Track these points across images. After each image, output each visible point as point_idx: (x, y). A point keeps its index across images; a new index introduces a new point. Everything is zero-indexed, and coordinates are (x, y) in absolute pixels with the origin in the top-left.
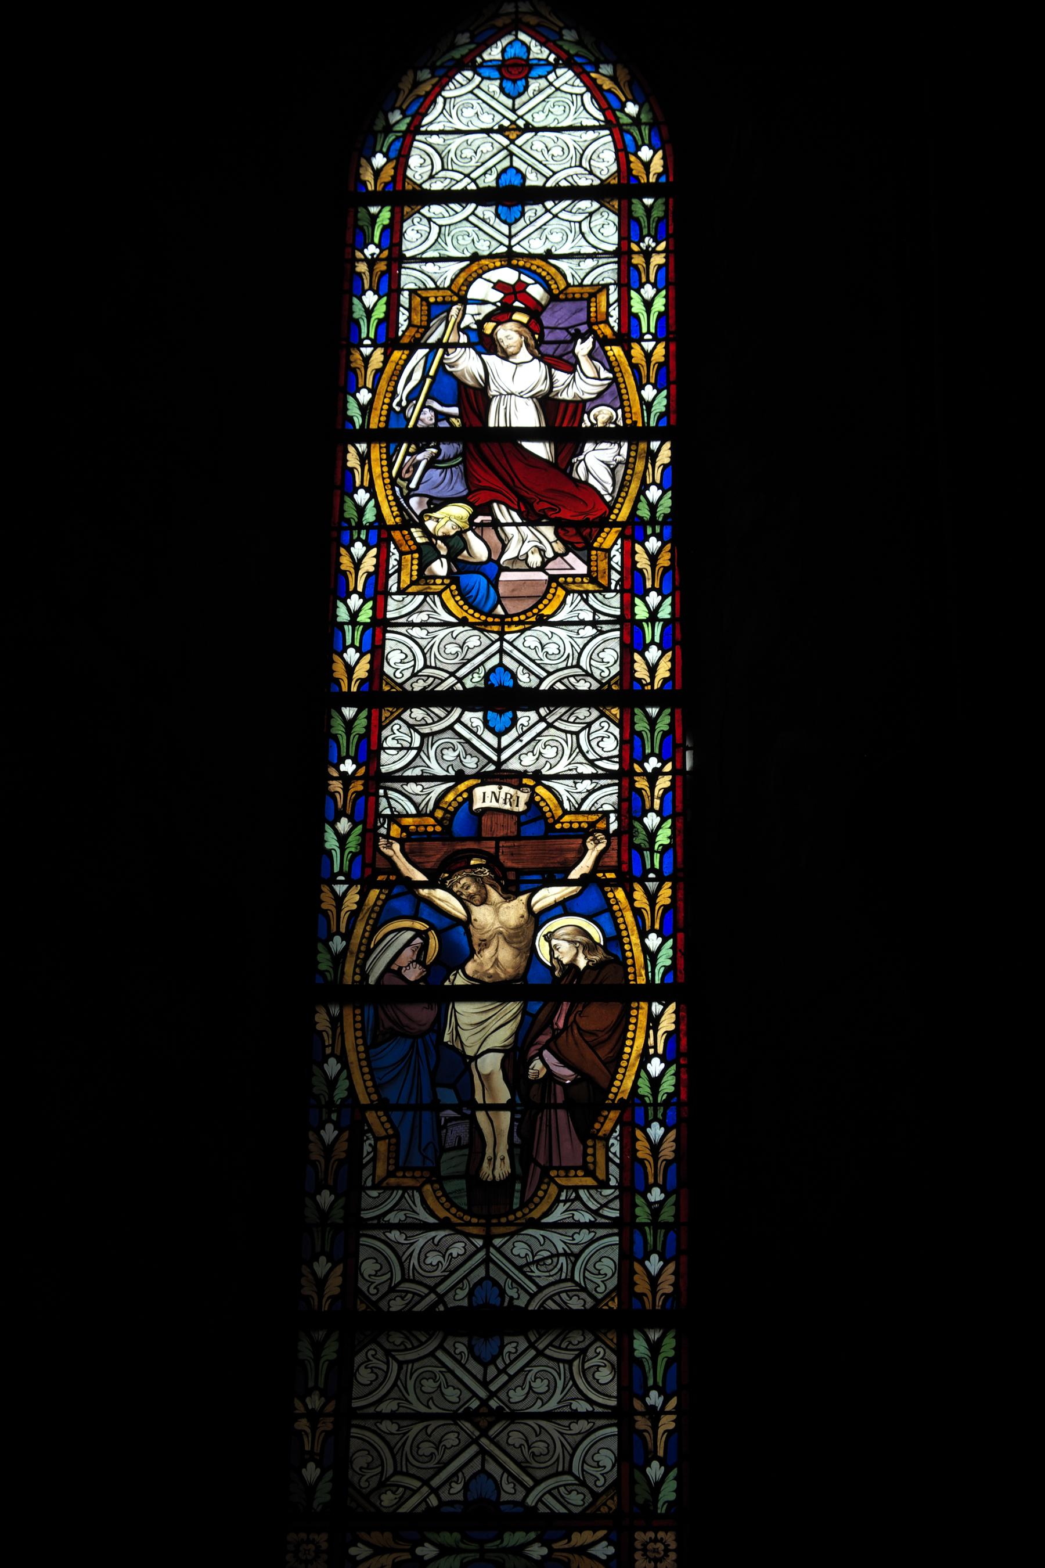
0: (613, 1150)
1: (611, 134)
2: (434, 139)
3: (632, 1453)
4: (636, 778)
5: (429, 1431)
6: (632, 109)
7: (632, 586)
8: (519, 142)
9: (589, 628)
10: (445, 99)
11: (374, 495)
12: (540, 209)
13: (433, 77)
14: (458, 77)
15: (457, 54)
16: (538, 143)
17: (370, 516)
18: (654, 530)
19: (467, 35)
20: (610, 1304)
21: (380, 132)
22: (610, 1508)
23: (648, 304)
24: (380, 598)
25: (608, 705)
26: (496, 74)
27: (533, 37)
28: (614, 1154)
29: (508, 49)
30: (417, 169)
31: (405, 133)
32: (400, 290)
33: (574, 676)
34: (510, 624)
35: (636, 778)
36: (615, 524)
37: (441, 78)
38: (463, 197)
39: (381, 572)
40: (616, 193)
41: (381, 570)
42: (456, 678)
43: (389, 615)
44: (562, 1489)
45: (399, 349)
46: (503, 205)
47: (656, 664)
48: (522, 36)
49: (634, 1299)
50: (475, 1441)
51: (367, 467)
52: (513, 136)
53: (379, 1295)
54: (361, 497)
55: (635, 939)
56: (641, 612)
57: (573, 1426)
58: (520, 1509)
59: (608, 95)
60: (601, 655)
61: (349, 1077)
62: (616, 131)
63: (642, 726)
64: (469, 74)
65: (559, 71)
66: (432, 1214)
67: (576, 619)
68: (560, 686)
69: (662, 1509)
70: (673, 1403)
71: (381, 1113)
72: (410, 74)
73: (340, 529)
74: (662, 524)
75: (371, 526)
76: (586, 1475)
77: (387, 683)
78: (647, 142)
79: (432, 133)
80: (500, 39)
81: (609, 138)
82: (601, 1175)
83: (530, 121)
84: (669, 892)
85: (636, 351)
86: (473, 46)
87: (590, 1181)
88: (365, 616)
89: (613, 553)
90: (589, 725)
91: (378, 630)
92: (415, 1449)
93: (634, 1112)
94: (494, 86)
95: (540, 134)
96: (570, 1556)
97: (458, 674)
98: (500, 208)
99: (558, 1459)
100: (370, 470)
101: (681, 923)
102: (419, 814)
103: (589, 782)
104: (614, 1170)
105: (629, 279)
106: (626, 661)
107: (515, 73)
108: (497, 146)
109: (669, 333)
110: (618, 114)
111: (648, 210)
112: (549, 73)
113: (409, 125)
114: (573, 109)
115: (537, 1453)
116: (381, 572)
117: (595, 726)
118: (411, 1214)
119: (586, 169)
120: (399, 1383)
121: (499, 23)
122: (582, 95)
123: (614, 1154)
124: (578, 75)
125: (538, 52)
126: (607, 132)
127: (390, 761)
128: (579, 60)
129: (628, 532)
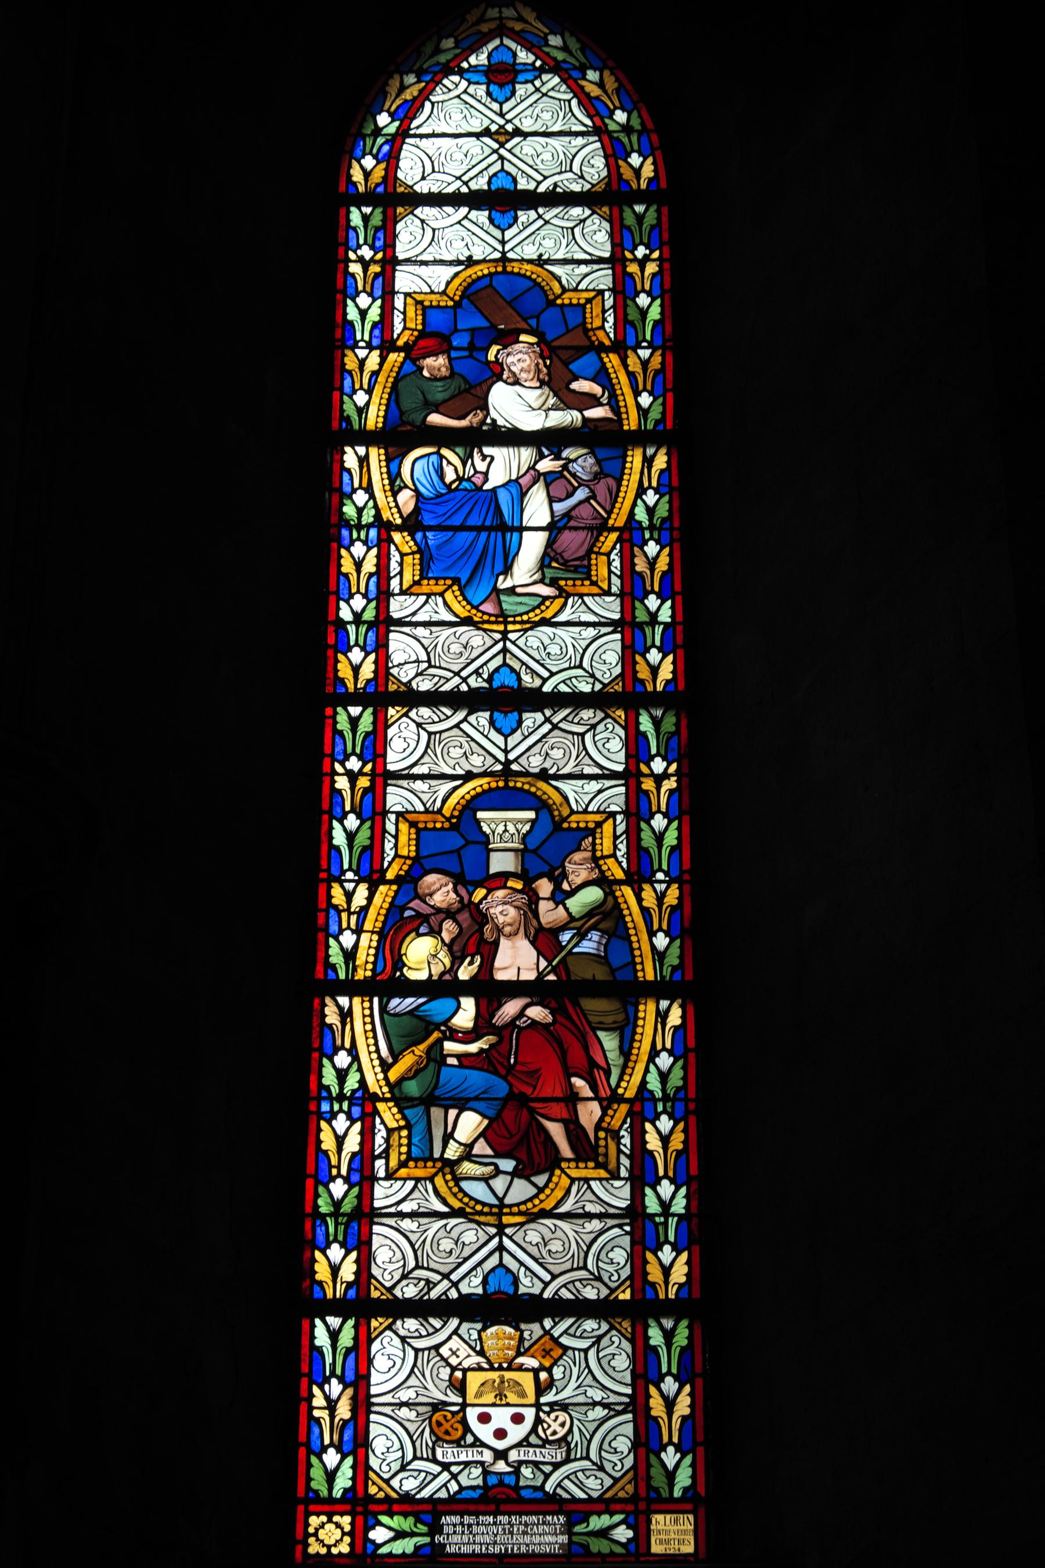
0: (614, 564)
1: (600, 140)
2: (424, 143)
3: (647, 1441)
4: (642, 779)
5: (448, 1228)
6: (621, 116)
7: (643, 1174)
8: (508, 146)
9: (598, 1409)
10: (433, 104)
11: (372, 496)
12: (533, 215)
13: (419, 81)
14: (445, 81)
15: (443, 58)
16: (528, 147)
17: (352, 1082)
18: (664, 1107)
19: (452, 40)
20: (616, 687)
21: (369, 135)
22: (627, 1493)
23: (670, 1404)
24: (384, 545)
25: (619, 1316)
26: (484, 79)
27: (518, 43)
28: (625, 1145)
29: (494, 54)
30: (410, 169)
31: (394, 136)
32: (385, 813)
33: (580, 1280)
34: (514, 623)
35: (642, 779)
36: (613, 529)
37: (427, 83)
38: (455, 200)
39: (365, 1156)
40: (607, 198)
41: (367, 1147)
42: (461, 677)
43: (377, 1204)
44: (580, 1475)
45: (394, 352)
46: (497, 211)
47: (673, 1268)
48: (507, 42)
49: (647, 1287)
50: (495, 151)
51: (365, 469)
52: (502, 139)
53: (392, 1472)
54: (361, 497)
55: (644, 936)
56: (652, 1205)
57: (586, 1225)
58: (539, 1495)
59: (596, 103)
60: (611, 1255)
61: (360, 1069)
62: (605, 138)
63: (656, 1337)
64: (456, 78)
65: (545, 77)
66: (445, 1202)
67: (581, 1211)
68: (563, 688)
69: (677, 1493)
70: (674, 767)
71: (405, 534)
72: (397, 77)
73: (319, 1099)
74: (660, 529)
75: (352, 1099)
76: (604, 1462)
77: (376, 1288)
78: (636, 147)
79: (421, 136)
80: (485, 44)
81: (598, 145)
82: (612, 1165)
83: (519, 125)
84: (686, 1332)
85: (632, 361)
86: (458, 51)
87: (603, 1173)
88: (369, 615)
89: (612, 557)
90: (593, 727)
91: (382, 628)
92: (435, 1245)
93: (631, 536)
94: (481, 91)
95: (529, 138)
96: (589, 1540)
97: (463, 178)
98: (493, 212)
99: (573, 1256)
100: (352, 1029)
101: (669, 386)
102: (427, 811)
103: (591, 629)
104: (625, 1161)
105: (644, 1234)
106: (637, 1260)
107: (502, 77)
108: (488, 151)
109: (664, 340)
110: (607, 121)
111: (640, 218)
112: (536, 78)
113: (398, 128)
114: (561, 115)
115: (554, 1250)
116: (382, 571)
117: (600, 728)
118: (423, 1203)
119: (594, 1464)
120: (416, 1370)
121: (485, 28)
122: (569, 101)
123: (625, 1145)
124: (564, 80)
125: (524, 56)
126: (596, 138)
127: (394, 761)
128: (564, 66)
129: (626, 536)
